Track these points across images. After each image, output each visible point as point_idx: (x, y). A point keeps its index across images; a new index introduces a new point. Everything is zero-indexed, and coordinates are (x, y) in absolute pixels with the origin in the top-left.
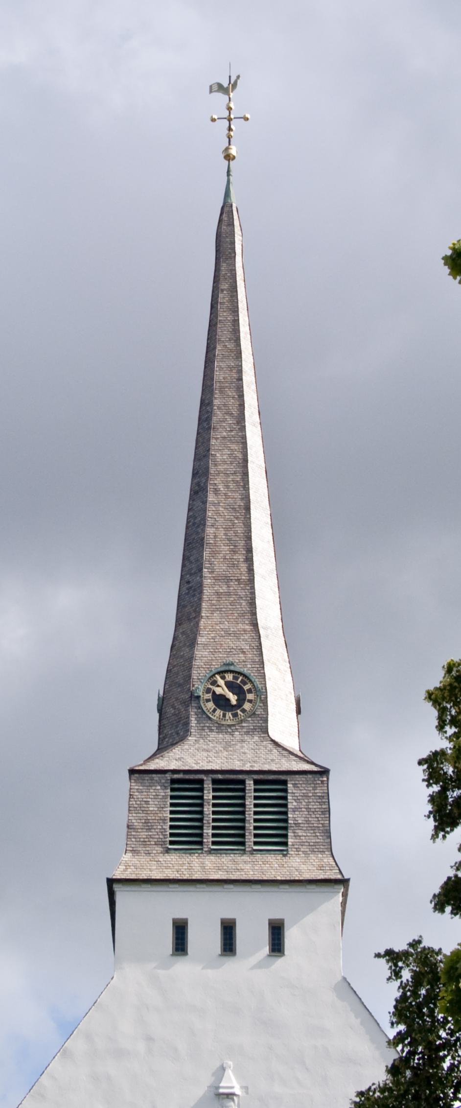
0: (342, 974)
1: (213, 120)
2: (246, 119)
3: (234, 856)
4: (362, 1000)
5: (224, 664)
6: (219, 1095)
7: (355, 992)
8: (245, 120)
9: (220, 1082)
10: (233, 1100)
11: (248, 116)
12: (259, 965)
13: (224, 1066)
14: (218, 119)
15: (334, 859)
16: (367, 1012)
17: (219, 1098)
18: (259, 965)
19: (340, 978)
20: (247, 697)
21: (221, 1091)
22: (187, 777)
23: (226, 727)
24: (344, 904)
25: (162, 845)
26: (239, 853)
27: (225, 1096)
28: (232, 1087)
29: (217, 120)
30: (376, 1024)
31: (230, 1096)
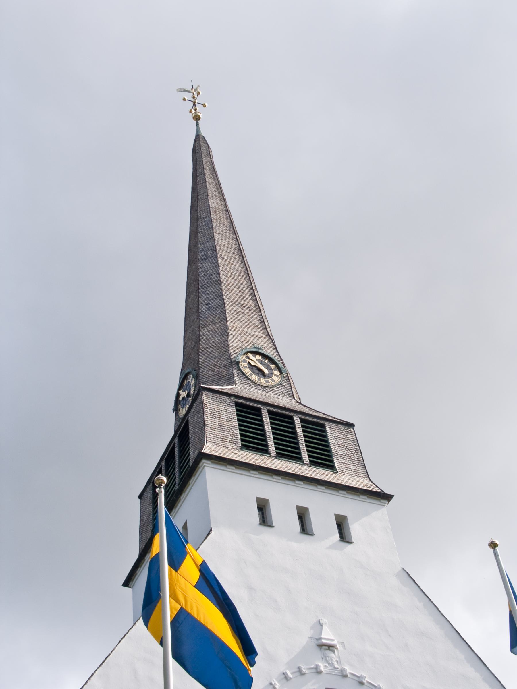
0: (401, 566)
1: (184, 100)
2: (204, 106)
3: (296, 465)
4: (421, 588)
5: (255, 347)
6: (321, 646)
7: (414, 581)
8: (204, 106)
9: (321, 635)
10: (334, 652)
11: (206, 104)
12: (333, 547)
13: (321, 622)
14: (187, 100)
15: (373, 483)
16: (427, 599)
17: (321, 649)
18: (333, 547)
19: (400, 569)
20: (274, 372)
21: (324, 641)
22: (184, 454)
23: (261, 387)
24: (192, 585)
25: (235, 444)
26: (299, 464)
27: (327, 647)
28: (333, 640)
29: (186, 101)
30: (436, 609)
31: (331, 648)
